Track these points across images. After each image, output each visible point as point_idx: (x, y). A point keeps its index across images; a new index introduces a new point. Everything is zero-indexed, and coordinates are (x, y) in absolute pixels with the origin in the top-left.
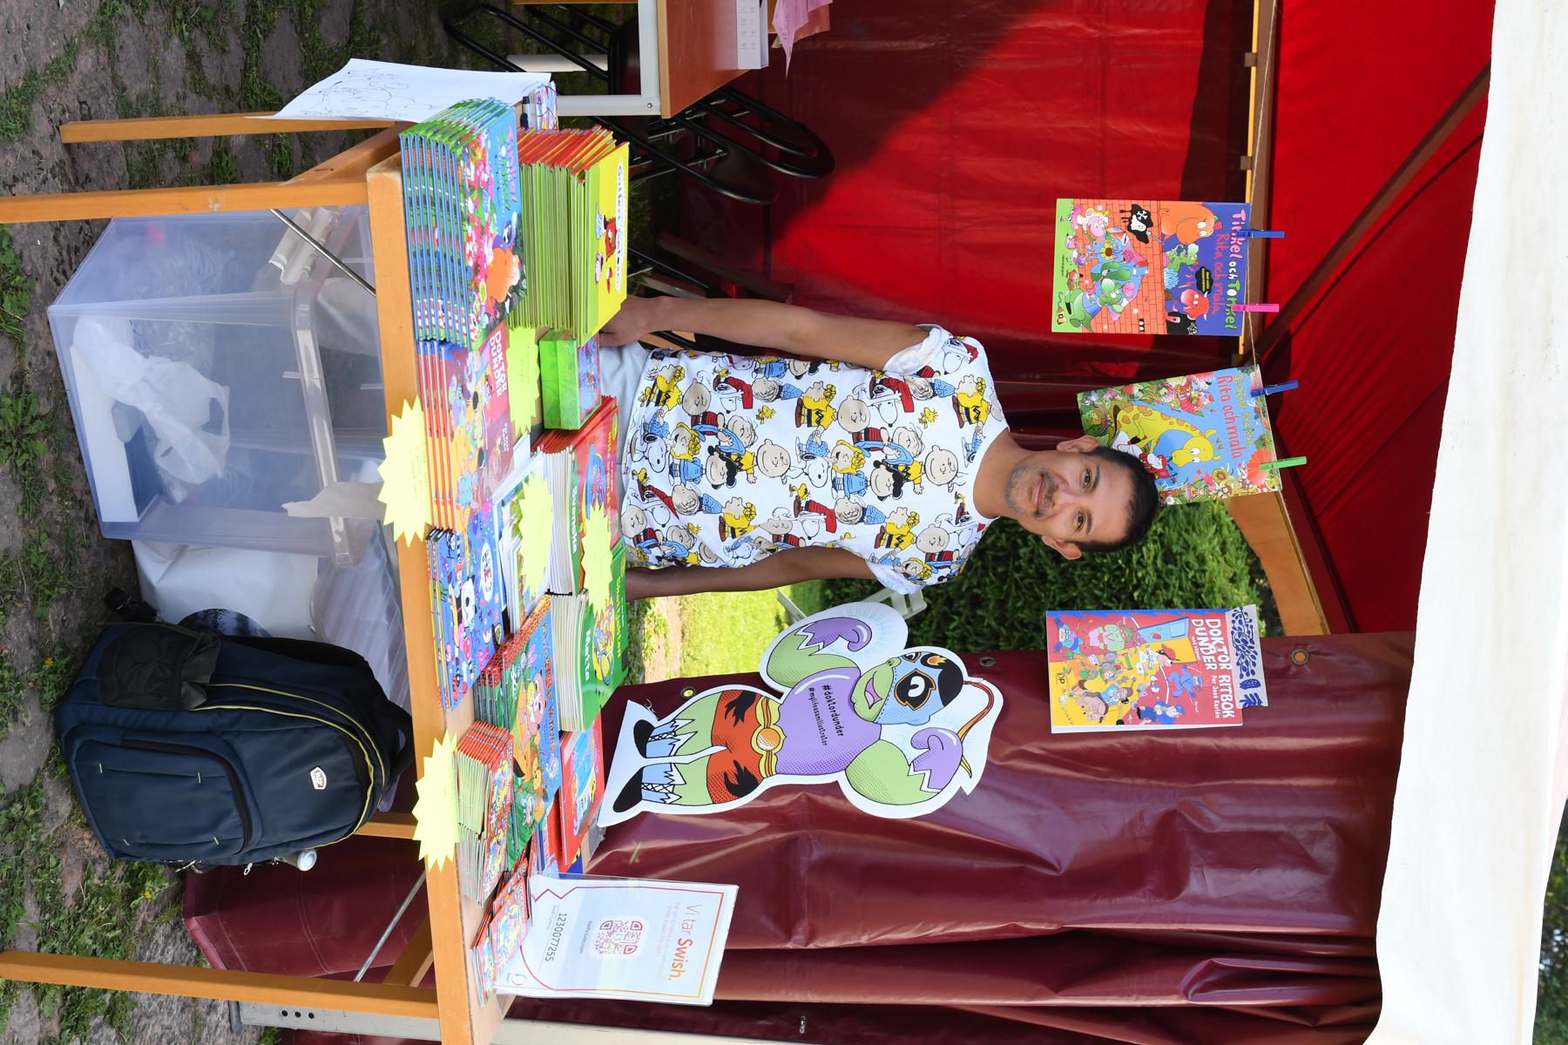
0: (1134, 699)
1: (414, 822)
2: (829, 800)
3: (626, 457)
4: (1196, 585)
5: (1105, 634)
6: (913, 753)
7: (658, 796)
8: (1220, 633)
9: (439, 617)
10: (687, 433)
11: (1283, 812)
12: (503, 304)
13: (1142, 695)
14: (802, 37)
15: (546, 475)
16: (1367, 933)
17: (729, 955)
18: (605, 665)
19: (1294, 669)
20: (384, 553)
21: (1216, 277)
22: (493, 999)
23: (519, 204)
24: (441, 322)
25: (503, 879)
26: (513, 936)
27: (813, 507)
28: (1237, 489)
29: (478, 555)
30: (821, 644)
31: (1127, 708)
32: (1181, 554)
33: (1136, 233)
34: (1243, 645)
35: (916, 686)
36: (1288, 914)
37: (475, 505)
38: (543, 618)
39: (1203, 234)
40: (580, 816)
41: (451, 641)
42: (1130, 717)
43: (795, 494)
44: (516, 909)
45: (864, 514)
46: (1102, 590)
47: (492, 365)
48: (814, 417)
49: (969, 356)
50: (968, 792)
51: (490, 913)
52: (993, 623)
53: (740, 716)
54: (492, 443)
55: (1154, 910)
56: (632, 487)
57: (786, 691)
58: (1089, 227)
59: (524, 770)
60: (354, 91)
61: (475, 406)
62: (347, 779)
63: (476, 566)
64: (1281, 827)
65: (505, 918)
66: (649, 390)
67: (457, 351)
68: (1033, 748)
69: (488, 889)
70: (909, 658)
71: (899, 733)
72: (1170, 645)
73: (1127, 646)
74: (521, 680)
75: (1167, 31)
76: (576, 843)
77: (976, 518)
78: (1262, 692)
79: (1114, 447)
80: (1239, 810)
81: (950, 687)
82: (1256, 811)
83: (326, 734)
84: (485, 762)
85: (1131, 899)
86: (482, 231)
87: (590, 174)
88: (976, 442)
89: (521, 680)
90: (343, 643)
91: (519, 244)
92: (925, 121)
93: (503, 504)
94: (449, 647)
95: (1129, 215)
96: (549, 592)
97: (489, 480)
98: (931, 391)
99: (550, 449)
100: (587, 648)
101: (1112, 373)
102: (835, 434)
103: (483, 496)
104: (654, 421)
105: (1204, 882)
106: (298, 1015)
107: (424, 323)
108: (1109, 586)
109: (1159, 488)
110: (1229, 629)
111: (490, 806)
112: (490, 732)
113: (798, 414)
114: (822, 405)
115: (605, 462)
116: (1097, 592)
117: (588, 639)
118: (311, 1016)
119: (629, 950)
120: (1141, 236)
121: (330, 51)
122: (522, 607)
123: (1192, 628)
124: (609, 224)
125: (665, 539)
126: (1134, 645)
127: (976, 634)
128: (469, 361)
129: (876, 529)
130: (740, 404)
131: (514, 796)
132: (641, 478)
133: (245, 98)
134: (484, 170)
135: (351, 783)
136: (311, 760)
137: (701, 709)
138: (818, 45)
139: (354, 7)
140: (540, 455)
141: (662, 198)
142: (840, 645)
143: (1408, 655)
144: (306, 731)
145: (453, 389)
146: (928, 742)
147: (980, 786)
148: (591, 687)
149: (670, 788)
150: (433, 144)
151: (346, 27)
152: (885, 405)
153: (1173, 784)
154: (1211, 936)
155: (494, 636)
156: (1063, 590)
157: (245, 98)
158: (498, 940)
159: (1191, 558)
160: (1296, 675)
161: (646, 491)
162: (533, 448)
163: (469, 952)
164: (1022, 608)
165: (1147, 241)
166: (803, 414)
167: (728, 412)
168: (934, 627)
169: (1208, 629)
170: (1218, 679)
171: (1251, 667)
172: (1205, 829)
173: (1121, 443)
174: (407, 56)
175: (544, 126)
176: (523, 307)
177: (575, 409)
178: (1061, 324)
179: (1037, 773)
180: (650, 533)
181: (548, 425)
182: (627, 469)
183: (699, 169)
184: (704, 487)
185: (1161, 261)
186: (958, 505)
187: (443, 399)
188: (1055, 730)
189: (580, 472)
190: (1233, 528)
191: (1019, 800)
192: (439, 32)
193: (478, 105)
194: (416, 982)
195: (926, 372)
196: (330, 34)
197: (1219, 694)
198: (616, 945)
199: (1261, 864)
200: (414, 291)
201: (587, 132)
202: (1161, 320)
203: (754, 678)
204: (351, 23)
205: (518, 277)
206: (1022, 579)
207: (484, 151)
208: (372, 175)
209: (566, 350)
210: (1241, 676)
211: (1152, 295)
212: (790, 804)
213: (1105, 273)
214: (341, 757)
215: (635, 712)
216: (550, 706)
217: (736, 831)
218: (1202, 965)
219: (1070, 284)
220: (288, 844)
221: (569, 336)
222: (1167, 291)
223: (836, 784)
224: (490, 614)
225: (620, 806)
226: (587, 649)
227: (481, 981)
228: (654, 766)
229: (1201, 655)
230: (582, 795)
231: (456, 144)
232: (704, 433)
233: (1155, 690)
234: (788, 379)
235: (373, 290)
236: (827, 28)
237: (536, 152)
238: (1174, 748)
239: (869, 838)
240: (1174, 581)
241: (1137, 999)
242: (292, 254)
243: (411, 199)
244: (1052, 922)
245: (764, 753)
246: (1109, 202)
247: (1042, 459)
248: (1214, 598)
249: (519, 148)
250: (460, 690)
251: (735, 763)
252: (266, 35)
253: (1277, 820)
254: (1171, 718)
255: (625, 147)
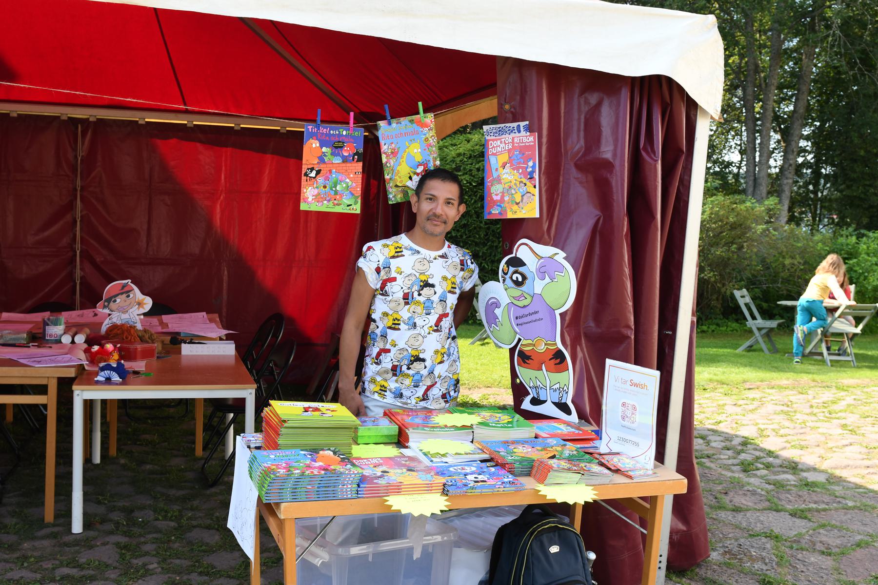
0: (524, 180)
1: (575, 504)
2: (568, 318)
3: (409, 406)
4: (470, 157)
5: (495, 193)
6: (547, 279)
7: (565, 395)
8: (495, 142)
9: (483, 490)
10: (400, 378)
11: (576, 116)
12: (341, 458)
13: (523, 177)
14: (221, 326)
15: (419, 442)
16: (630, 80)
17: (637, 363)
18: (505, 418)
19: (512, 110)
20: (451, 518)
21: (337, 139)
22: (656, 471)
23: (295, 450)
24: (349, 486)
25: (602, 464)
26: (628, 461)
27: (437, 324)
28: (433, 133)
29: (455, 473)
30: (497, 320)
31: (528, 183)
32: (456, 164)
33: (316, 175)
34: (501, 132)
35: (517, 278)
36: (621, 114)
37: (433, 473)
38: (484, 444)
39: (318, 145)
40: (573, 430)
41: (494, 486)
42: (533, 182)
43: (431, 332)
44: (616, 459)
45: (443, 301)
46: (472, 199)
47: (369, 464)
48: (396, 322)
49: (371, 250)
50: (565, 255)
51: (617, 471)
52: (486, 248)
53: (529, 358)
54: (404, 465)
55: (619, 174)
56: (423, 404)
57: (518, 336)
58: (313, 196)
59: (552, 454)
60: (243, 525)
61: (388, 472)
62: (555, 536)
63: (460, 474)
64: (583, 117)
65: (619, 464)
66: (379, 395)
67: (363, 479)
68: (545, 227)
69: (607, 471)
70: (504, 281)
71: (538, 286)
72: (500, 164)
73: (501, 183)
74: (512, 455)
75: (223, 164)
76: (585, 432)
77: (445, 249)
78: (522, 124)
79: (414, 188)
80: (575, 135)
81: (517, 262)
82: (575, 128)
83: (534, 545)
84: (549, 472)
85: (614, 184)
86: (308, 467)
87: (283, 417)
88: (411, 249)
89: (512, 455)
90: (493, 537)
91: (314, 451)
92: (260, 272)
93: (432, 461)
94: (497, 487)
95: (308, 178)
96: (472, 442)
97: (422, 467)
98: (387, 269)
99: (407, 440)
100: (498, 425)
101: (376, 191)
102: (405, 313)
103: (428, 470)
104: (394, 393)
105: (607, 151)
106: (660, 562)
107: (349, 494)
108: (469, 196)
109: (432, 168)
110: (494, 138)
111: (569, 469)
112: (535, 469)
113: (394, 329)
114: (391, 318)
115: (413, 415)
116: (472, 202)
117: (494, 425)
118: (661, 556)
119: (635, 408)
120: (318, 172)
121: (222, 539)
122: (478, 453)
123: (493, 154)
124: (306, 410)
125: (447, 389)
126: (500, 180)
127: (490, 256)
128: (367, 474)
129: (449, 295)
130: (388, 354)
131: (564, 459)
132: (418, 400)
133: (242, 577)
134: (281, 465)
135: (557, 534)
136: (546, 552)
137: (526, 375)
138: (224, 320)
139: (202, 527)
140: (410, 444)
141: (291, 392)
142: (498, 312)
143: (507, 60)
144: (532, 554)
145: (380, 482)
146: (542, 273)
147: (562, 250)
148: (515, 424)
149: (561, 389)
150: (269, 488)
151: (211, 531)
152: (392, 290)
153: (563, 164)
154: (631, 146)
155: (492, 466)
156: (471, 216)
157: (242, 577)
158: (630, 468)
159: (458, 159)
160: (515, 109)
161: (425, 398)
162: (407, 447)
163: (635, 480)
164: (479, 235)
165: (320, 170)
166: (395, 327)
167: (392, 360)
168: (487, 275)
169: (494, 147)
170: (516, 143)
171: (511, 128)
172: (583, 150)
173: (413, 184)
174: (226, 505)
175: (261, 439)
176: (343, 450)
177: (389, 428)
178: (357, 209)
179: (557, 225)
180: (444, 396)
181: (396, 441)
182: (414, 406)
183: (279, 374)
184: (425, 372)
185: (329, 164)
186: (439, 258)
187: (384, 487)
188: (537, 216)
189: (418, 426)
190: (445, 141)
191: (569, 232)
192: (213, 490)
193: (251, 467)
194: (648, 506)
195: (378, 270)
196: (213, 538)
197: (523, 143)
198: (633, 414)
199: (599, 126)
200: (335, 498)
201: (264, 419)
202: (356, 164)
203: (512, 351)
204: (209, 529)
205: (329, 452)
206: (466, 235)
207: (273, 465)
208: (282, 517)
209: (362, 432)
210: (515, 133)
211: (345, 168)
212: (569, 335)
213: (334, 189)
214: (545, 539)
215: (526, 405)
216: (523, 442)
217: (581, 360)
218: (643, 153)
219: (338, 205)
220: (584, 564)
221: (356, 429)
222: (343, 162)
223: (560, 314)
224: (482, 468)
225: (569, 412)
226: (498, 425)
227: (648, 475)
228: (550, 396)
229: (505, 150)
230: (564, 429)
231: (269, 477)
232: (401, 371)
233: (521, 171)
234: (378, 331)
235: (334, 517)
236: (217, 315)
237: (272, 442)
238: (547, 163)
239: (585, 301)
240: (468, 167)
241: (658, 182)
242: (316, 556)
243: (293, 499)
244: (624, 219)
245: (546, 346)
246: (302, 186)
247: (420, 219)
248: (476, 149)
249: (270, 449)
250: (516, 482)
251: (550, 360)
252: (213, 567)
253: (579, 119)
254: (533, 164)
255: (272, 402)
